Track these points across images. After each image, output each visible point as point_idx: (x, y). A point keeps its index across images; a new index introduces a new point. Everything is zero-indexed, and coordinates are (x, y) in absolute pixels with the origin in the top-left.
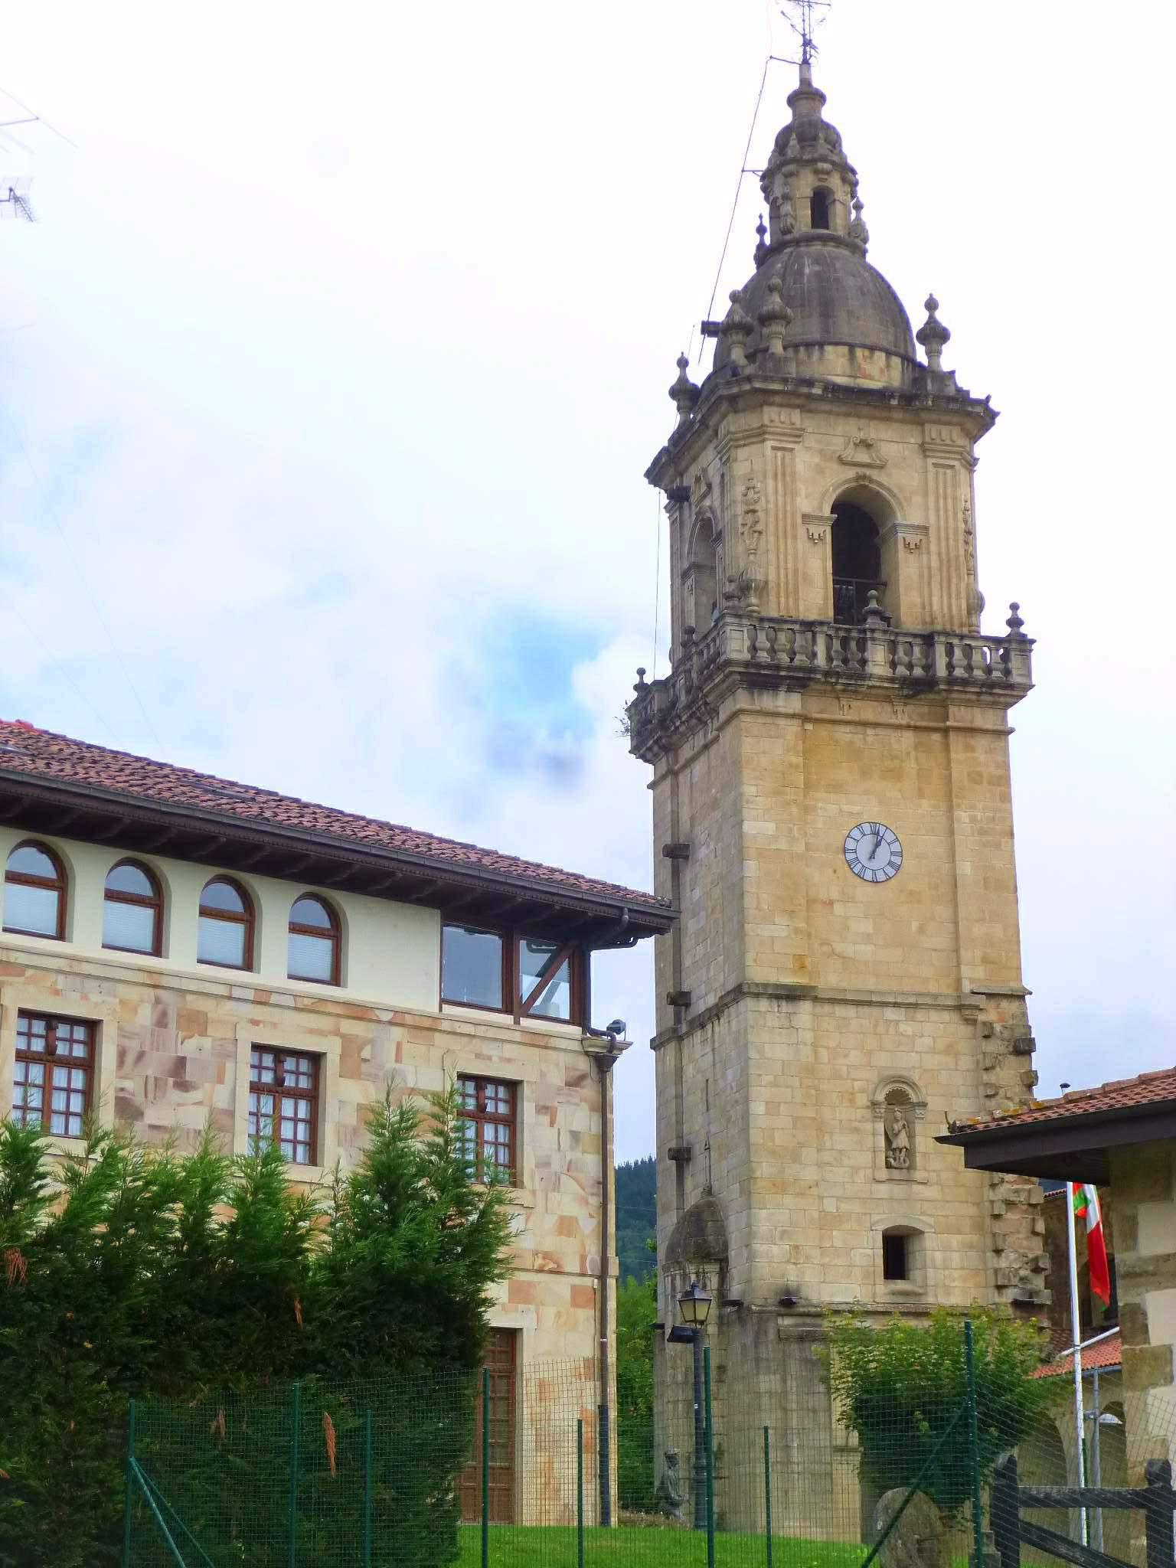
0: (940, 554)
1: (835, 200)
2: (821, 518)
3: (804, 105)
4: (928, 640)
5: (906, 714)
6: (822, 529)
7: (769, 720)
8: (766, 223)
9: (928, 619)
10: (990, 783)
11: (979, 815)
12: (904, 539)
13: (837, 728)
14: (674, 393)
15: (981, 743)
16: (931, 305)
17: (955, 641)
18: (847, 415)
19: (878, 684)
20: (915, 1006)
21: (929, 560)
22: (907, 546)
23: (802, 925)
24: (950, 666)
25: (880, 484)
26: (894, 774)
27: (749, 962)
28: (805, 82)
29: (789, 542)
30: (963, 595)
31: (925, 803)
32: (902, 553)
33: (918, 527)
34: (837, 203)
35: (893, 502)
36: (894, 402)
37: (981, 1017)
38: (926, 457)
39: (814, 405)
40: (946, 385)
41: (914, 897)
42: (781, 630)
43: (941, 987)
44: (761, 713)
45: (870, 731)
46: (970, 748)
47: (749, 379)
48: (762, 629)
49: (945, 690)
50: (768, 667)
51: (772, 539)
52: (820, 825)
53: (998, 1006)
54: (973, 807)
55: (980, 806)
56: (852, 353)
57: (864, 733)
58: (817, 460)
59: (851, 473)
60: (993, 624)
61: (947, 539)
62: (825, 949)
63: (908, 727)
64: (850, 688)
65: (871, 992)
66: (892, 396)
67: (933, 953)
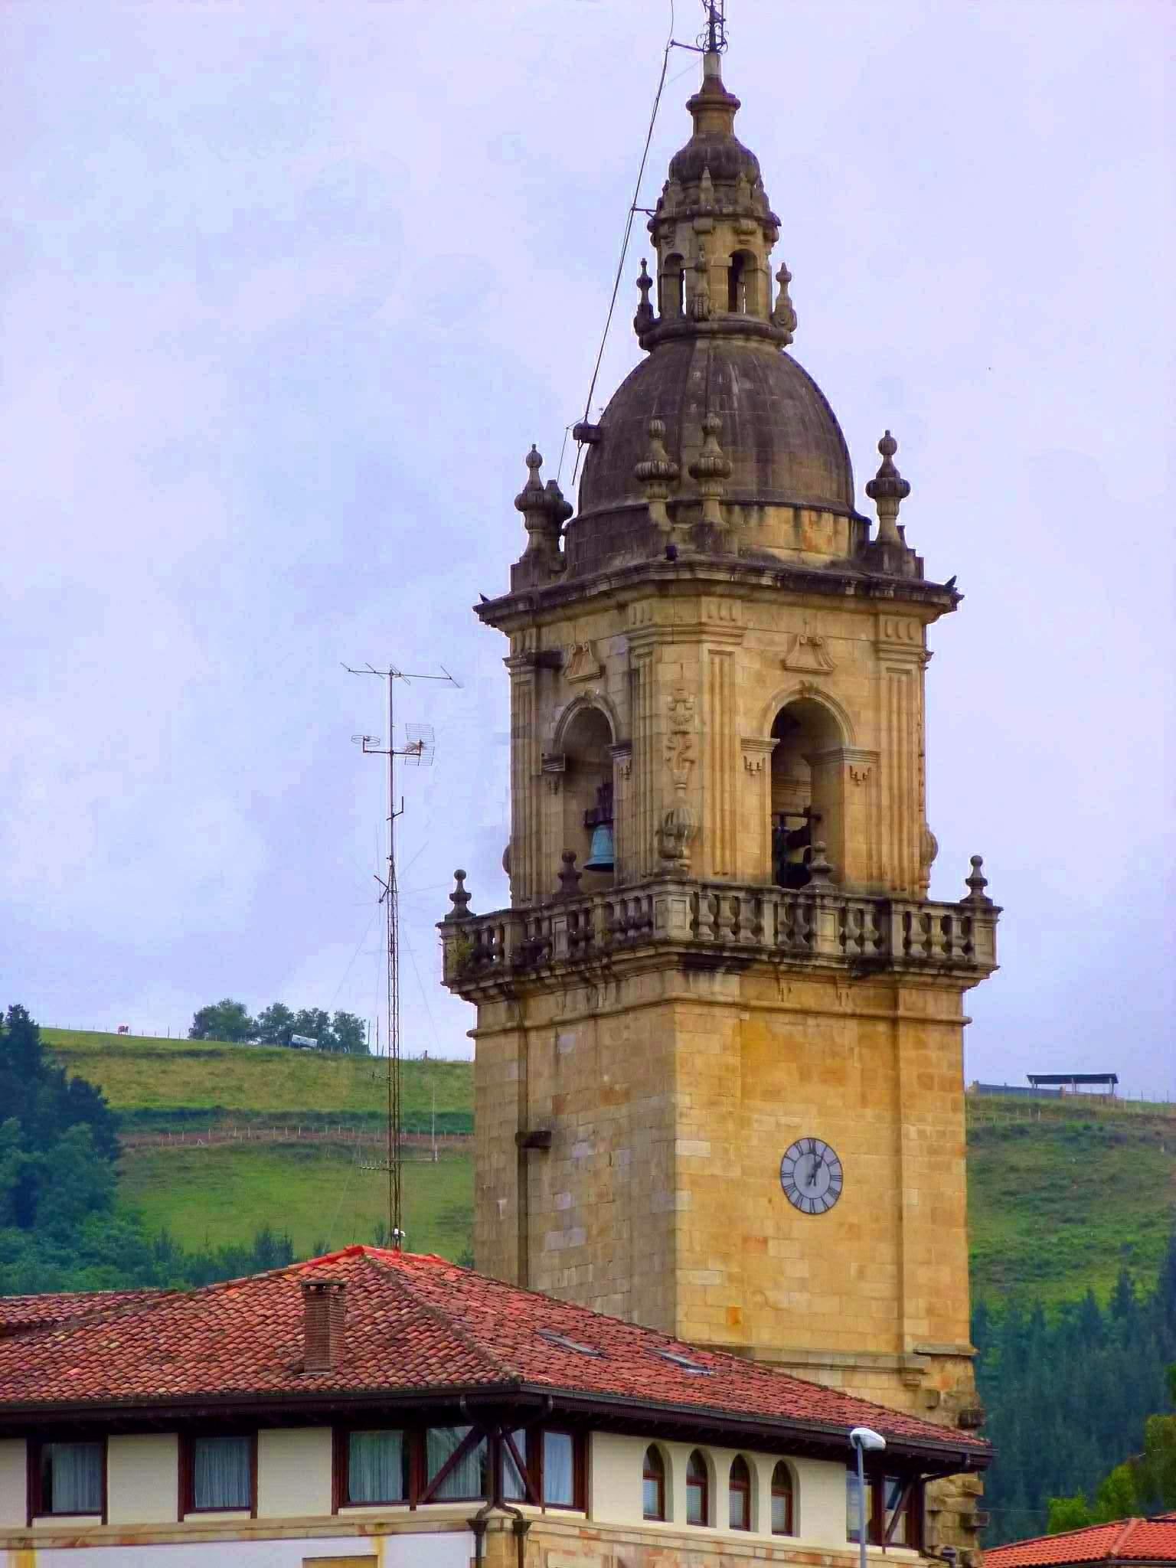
0: (891, 788)
1: (755, 270)
2: (761, 743)
3: (713, 120)
4: (883, 908)
5: (850, 998)
6: (761, 756)
7: (705, 1010)
8: (653, 272)
9: (875, 872)
10: (943, 1088)
11: (928, 1129)
12: (851, 768)
13: (775, 1016)
14: (522, 504)
15: (934, 1035)
16: (887, 447)
17: (913, 909)
18: (792, 604)
19: (825, 964)
20: (854, 1368)
21: (879, 796)
22: (854, 777)
23: (735, 1269)
24: (907, 943)
25: (828, 697)
26: (835, 1077)
27: (680, 1315)
28: (712, 81)
29: (727, 776)
30: (916, 842)
31: (869, 1112)
32: (848, 786)
33: (871, 753)
34: (759, 272)
35: (839, 718)
36: (850, 591)
37: (926, 1383)
38: (878, 659)
39: (757, 595)
40: (904, 562)
41: (854, 1231)
42: (725, 898)
43: (879, 1344)
44: (701, 1002)
45: (811, 1021)
46: (920, 1044)
47: (691, 566)
48: (705, 897)
49: (898, 972)
50: (713, 947)
51: (707, 772)
52: (755, 1142)
53: (942, 1369)
54: (922, 1120)
55: (929, 1117)
56: (797, 518)
57: (804, 1024)
58: (757, 666)
59: (793, 683)
61: (899, 768)
62: (758, 1298)
63: (853, 1016)
64: (794, 969)
65: (808, 1353)
66: (849, 584)
67: (873, 1302)
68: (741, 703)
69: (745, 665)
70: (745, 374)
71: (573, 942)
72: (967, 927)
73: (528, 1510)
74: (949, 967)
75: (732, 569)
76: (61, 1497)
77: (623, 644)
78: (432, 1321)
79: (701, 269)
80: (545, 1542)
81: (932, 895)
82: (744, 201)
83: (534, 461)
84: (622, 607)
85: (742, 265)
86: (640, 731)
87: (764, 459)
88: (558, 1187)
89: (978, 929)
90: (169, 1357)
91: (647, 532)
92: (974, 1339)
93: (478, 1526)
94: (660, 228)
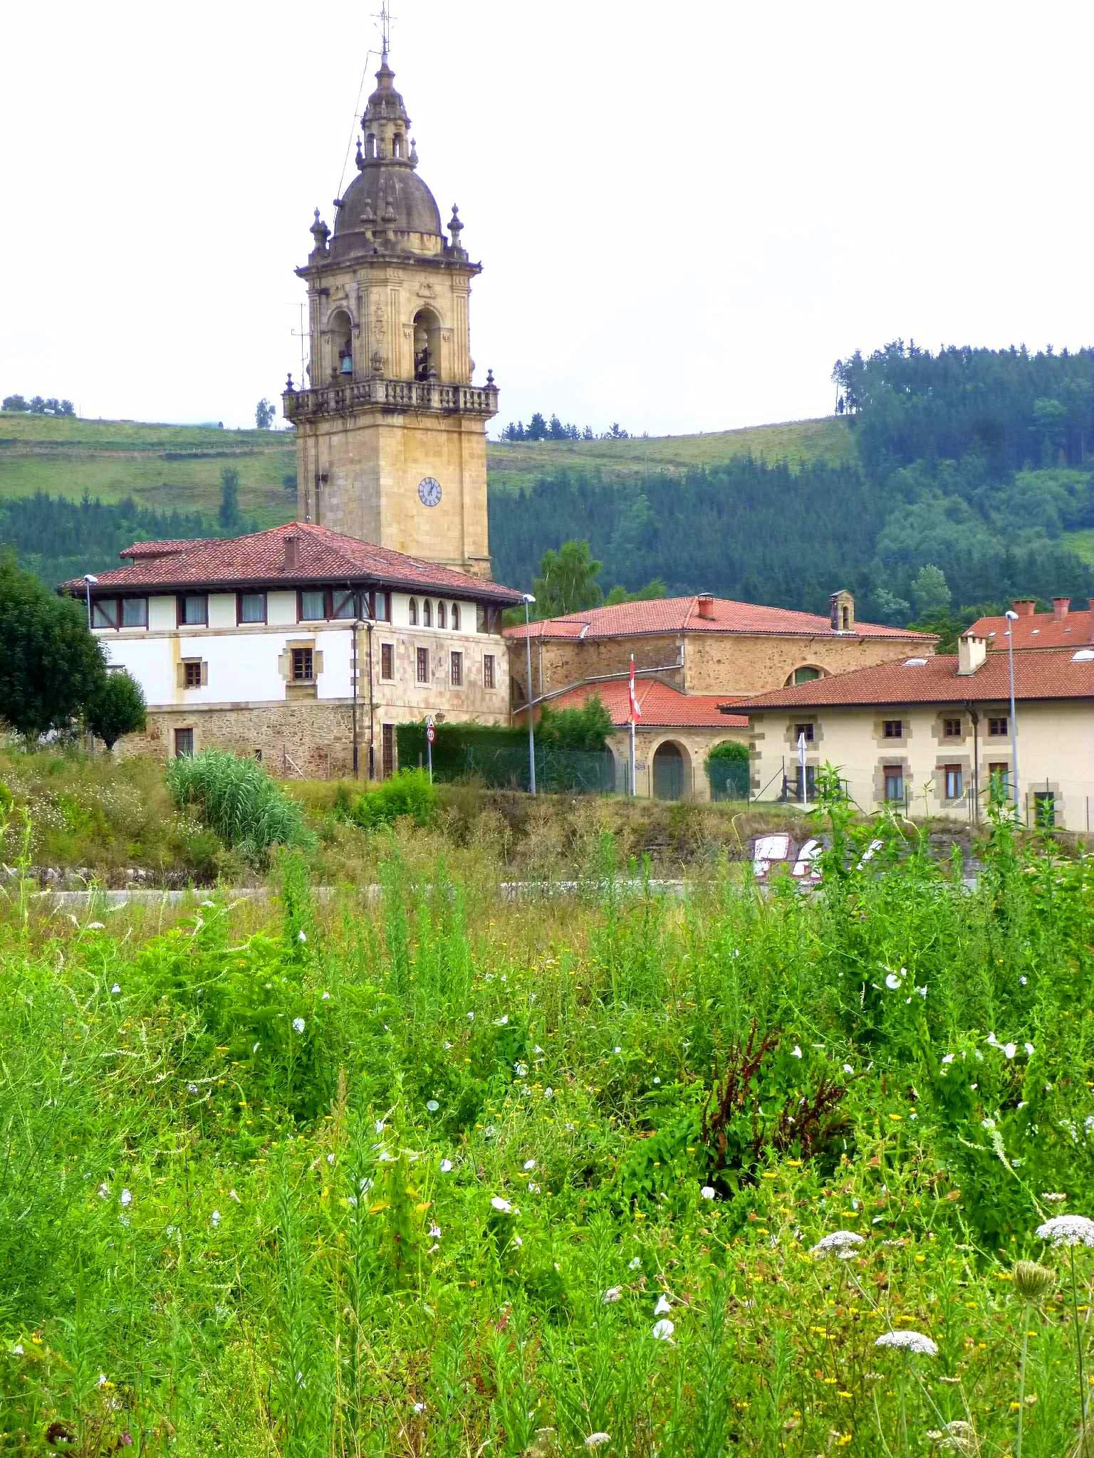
3: (385, 80)
4: (456, 389)
8: (362, 141)
14: (312, 230)
16: (455, 210)
26: (438, 454)
28: (384, 66)
31: (451, 468)
37: (472, 570)
41: (446, 513)
46: (469, 441)
47: (383, 256)
59: (421, 302)
60: (479, 381)
68: (402, 310)
69: (403, 295)
70: (400, 181)
71: (337, 402)
72: (487, 396)
73: (372, 622)
74: (480, 412)
75: (398, 257)
76: (189, 617)
77: (355, 286)
78: (329, 550)
79: (382, 140)
80: (378, 634)
81: (474, 384)
82: (398, 113)
83: (317, 214)
84: (355, 272)
85: (398, 137)
86: (363, 320)
87: (409, 214)
88: (331, 496)
89: (491, 397)
90: (230, 565)
91: (365, 243)
92: (490, 552)
93: (354, 628)
94: (365, 123)
